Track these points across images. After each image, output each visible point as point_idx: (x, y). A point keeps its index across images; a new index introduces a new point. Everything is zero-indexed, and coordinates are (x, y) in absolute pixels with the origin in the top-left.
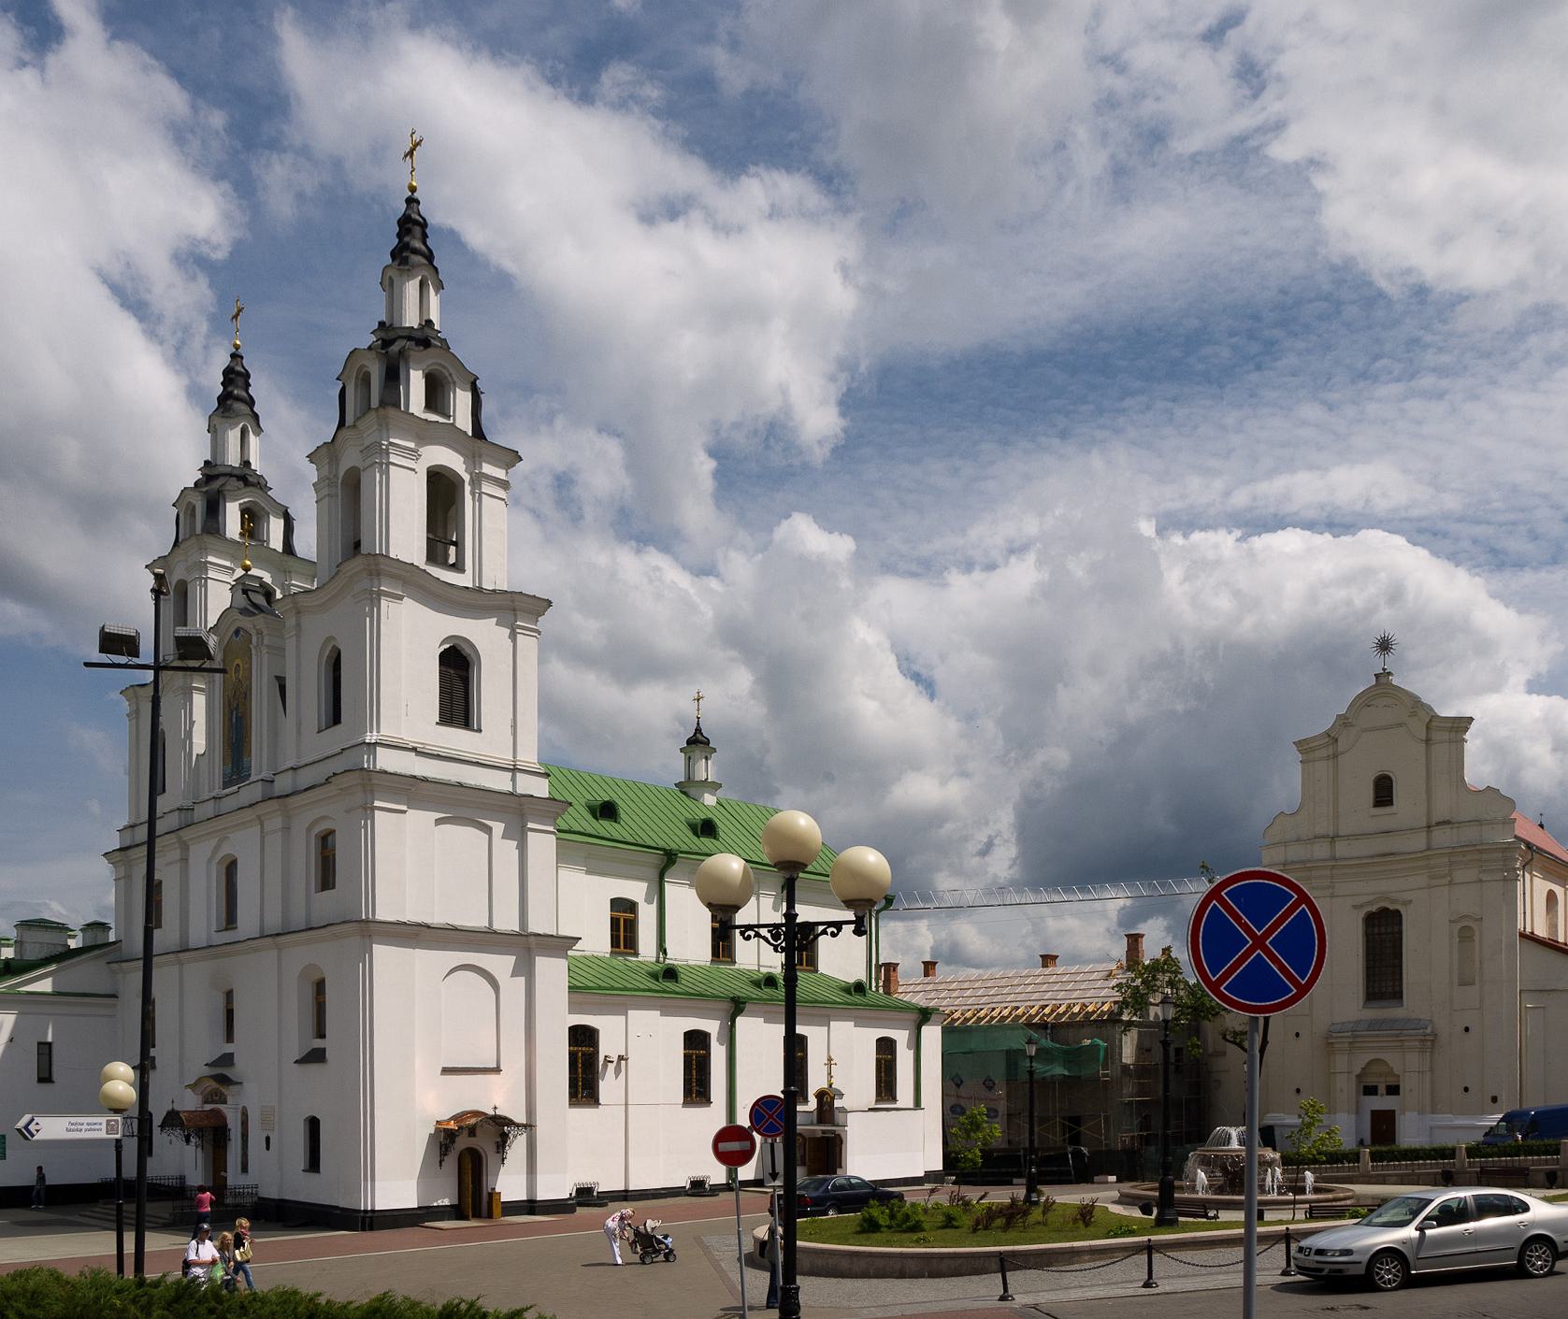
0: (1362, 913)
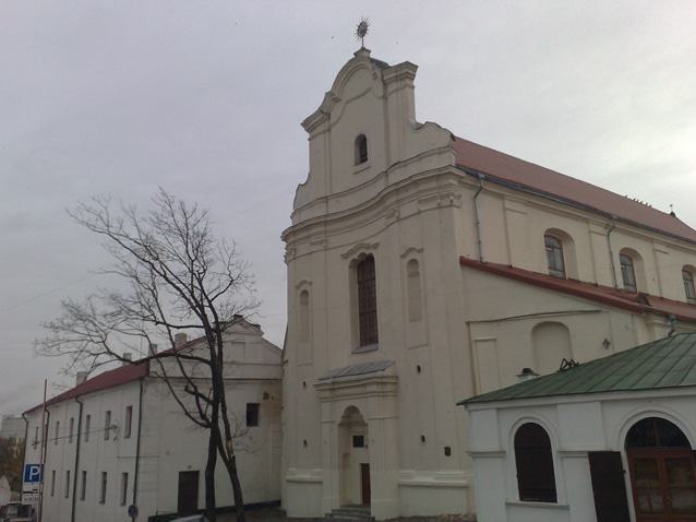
0: (348, 262)
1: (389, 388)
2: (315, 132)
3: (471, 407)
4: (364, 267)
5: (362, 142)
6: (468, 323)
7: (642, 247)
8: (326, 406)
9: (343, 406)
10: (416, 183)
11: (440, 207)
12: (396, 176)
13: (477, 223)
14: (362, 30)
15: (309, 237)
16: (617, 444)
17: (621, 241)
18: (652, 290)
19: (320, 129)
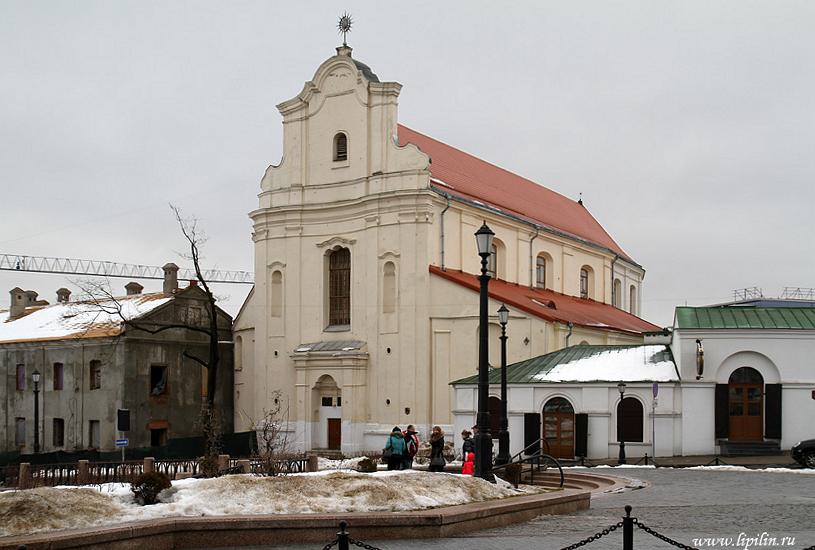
1: (362, 363)
2: (290, 118)
3: (457, 387)
4: (339, 259)
5: (341, 140)
6: (431, 319)
7: (554, 250)
8: (301, 374)
9: (317, 375)
10: (398, 198)
11: (417, 222)
12: (377, 186)
13: (443, 236)
14: (345, 25)
15: (284, 221)
16: (539, 410)
17: (540, 246)
18: (557, 289)
19: (297, 115)
